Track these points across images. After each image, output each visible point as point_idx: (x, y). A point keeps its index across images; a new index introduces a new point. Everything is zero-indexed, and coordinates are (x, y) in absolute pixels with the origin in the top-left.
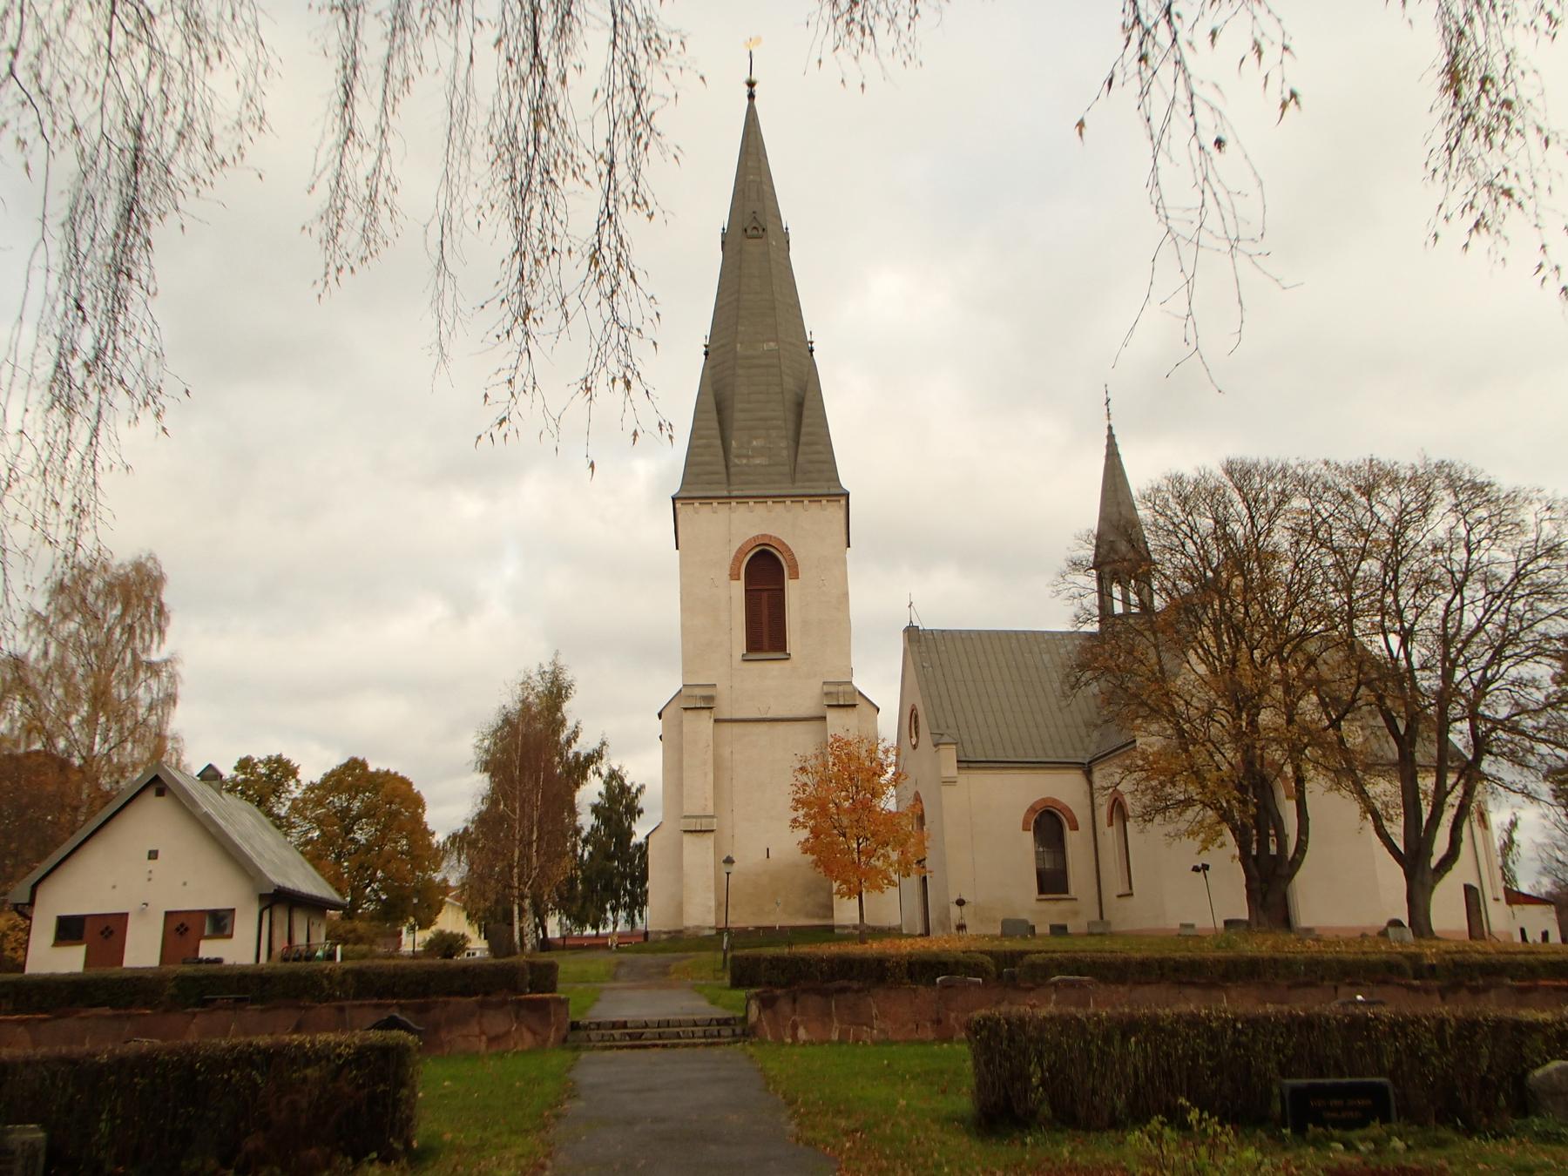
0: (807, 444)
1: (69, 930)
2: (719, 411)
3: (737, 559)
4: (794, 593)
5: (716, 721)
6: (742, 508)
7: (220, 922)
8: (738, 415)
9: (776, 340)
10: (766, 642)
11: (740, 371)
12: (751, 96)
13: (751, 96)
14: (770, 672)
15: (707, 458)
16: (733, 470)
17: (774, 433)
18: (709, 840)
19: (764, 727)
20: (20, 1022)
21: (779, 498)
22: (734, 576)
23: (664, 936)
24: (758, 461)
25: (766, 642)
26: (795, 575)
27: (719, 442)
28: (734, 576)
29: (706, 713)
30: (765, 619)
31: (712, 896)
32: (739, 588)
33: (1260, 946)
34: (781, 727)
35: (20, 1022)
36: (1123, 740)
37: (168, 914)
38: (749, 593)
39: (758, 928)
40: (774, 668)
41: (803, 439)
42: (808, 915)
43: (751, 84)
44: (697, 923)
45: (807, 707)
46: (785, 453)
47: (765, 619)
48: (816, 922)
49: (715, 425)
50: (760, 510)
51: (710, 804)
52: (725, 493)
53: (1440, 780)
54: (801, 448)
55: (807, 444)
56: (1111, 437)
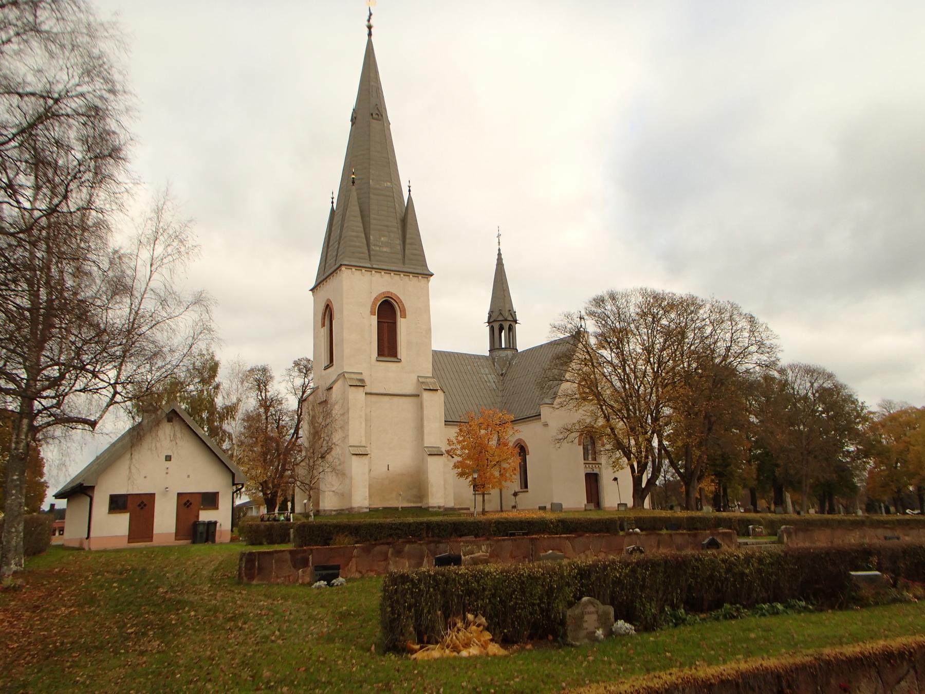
0: (411, 244)
1: (117, 503)
2: (362, 217)
3: (374, 303)
4: (403, 326)
5: (366, 394)
6: (378, 275)
7: (211, 500)
8: (372, 221)
9: (391, 182)
10: (386, 352)
11: (372, 196)
12: (370, 34)
13: (370, 34)
14: (389, 368)
15: (357, 244)
16: (372, 253)
17: (392, 235)
18: (365, 460)
19: (386, 399)
20: (568, 538)
21: (397, 272)
22: (372, 313)
23: (334, 513)
24: (385, 250)
25: (386, 352)
26: (404, 316)
27: (363, 235)
28: (372, 313)
29: (361, 389)
30: (386, 339)
31: (367, 490)
32: (374, 319)
33: (595, 515)
34: (396, 399)
35: (568, 538)
36: (533, 412)
37: (179, 494)
38: (379, 323)
39: (384, 508)
40: (392, 366)
41: (408, 241)
42: (409, 501)
43: (370, 27)
44: (359, 505)
45: (410, 388)
46: (399, 247)
47: (386, 339)
48: (412, 505)
49: (361, 225)
50: (387, 277)
51: (363, 439)
52: (369, 266)
53: (636, 440)
54: (407, 246)
55: (411, 244)
56: (500, 254)
